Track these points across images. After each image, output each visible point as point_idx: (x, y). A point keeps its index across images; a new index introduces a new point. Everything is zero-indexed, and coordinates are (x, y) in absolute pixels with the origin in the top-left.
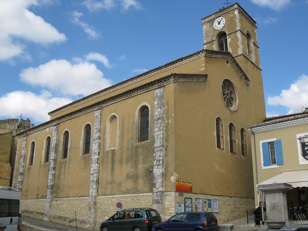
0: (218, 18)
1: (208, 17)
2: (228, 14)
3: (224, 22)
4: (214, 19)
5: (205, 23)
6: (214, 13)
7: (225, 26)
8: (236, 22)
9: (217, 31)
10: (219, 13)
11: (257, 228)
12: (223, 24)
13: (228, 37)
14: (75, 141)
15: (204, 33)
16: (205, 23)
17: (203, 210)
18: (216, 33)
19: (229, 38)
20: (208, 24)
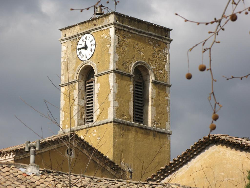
0: (85, 36)
1: (70, 27)
2: (100, 33)
3: (93, 42)
4: (79, 35)
5: (65, 40)
6: (79, 22)
7: (94, 56)
8: (109, 53)
9: (83, 62)
10: (87, 24)
11: (79, 127)
12: (92, 45)
13: (96, 79)
14: (132, 164)
15: (62, 60)
16: (65, 40)
17: (82, 185)
18: (79, 68)
19: (97, 82)
20: (69, 43)
